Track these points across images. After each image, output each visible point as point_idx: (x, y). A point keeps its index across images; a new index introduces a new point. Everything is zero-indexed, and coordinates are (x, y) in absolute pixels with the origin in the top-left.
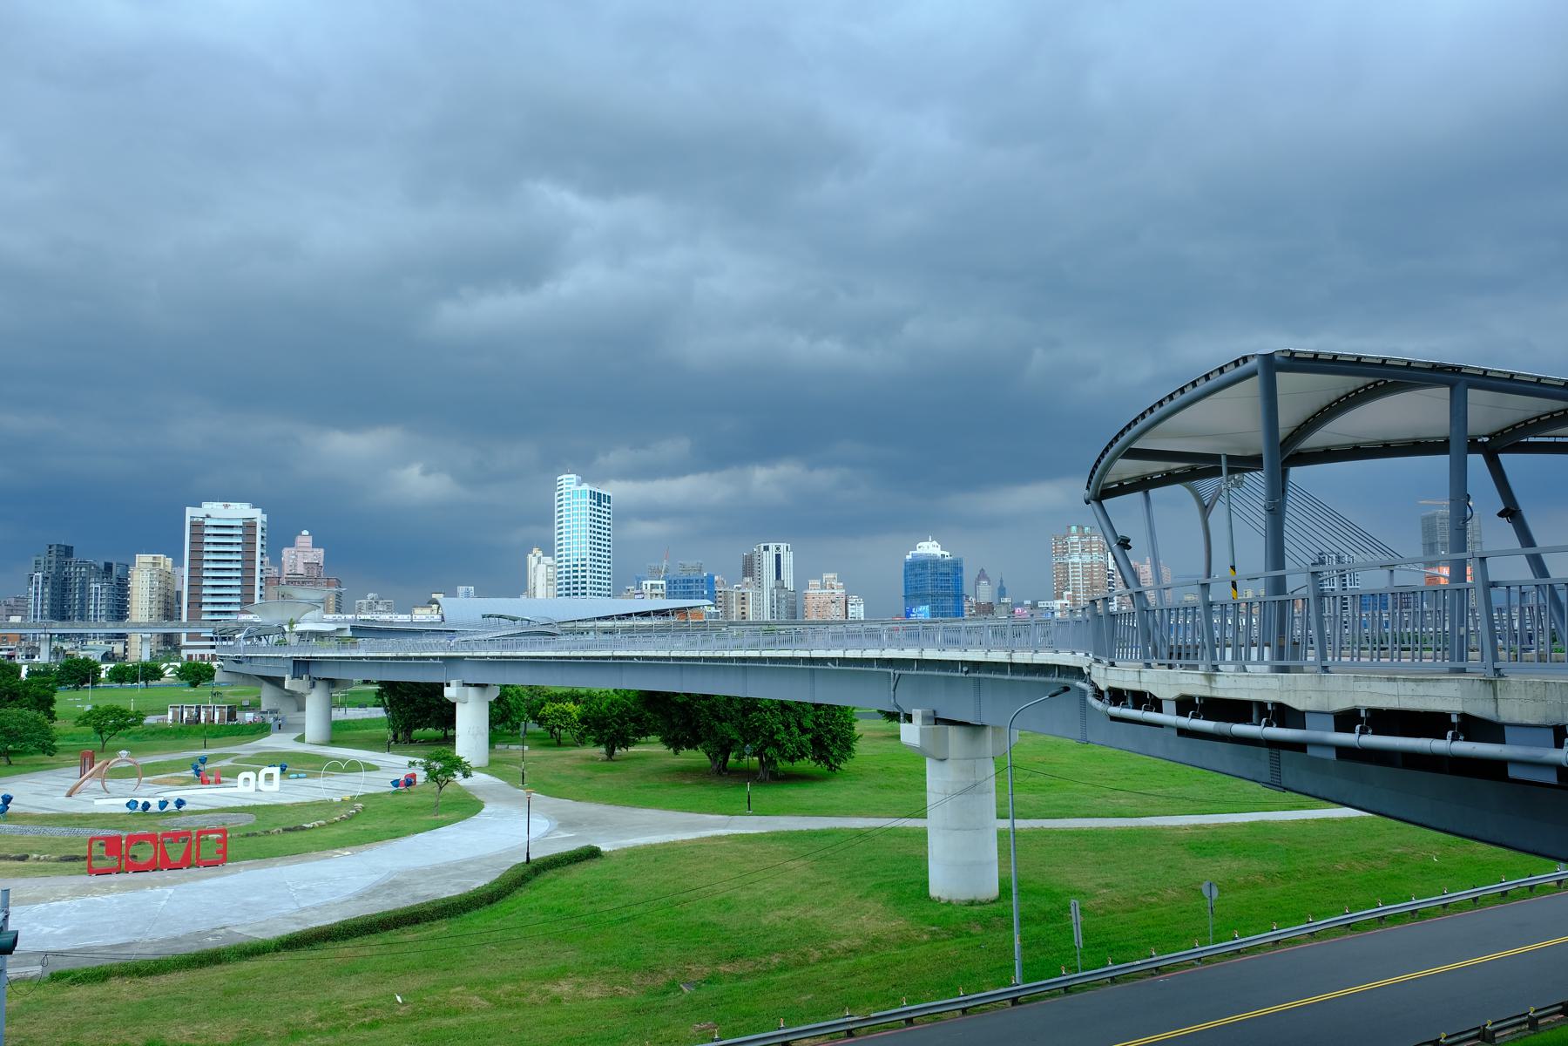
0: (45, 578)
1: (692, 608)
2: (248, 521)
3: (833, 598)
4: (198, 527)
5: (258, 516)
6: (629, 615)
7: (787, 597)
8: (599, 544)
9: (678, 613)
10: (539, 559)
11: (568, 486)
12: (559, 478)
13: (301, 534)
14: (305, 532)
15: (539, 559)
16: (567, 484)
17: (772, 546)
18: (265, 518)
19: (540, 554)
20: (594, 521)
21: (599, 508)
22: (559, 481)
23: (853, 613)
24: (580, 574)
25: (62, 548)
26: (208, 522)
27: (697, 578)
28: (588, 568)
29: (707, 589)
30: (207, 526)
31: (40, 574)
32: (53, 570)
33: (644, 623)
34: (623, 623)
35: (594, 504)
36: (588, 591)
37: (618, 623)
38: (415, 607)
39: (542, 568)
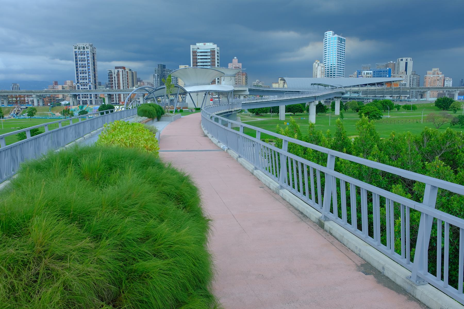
0: (158, 75)
1: (393, 81)
2: (212, 50)
3: (438, 78)
4: (194, 52)
5: (215, 46)
6: (366, 85)
7: (417, 79)
8: (341, 58)
9: (387, 84)
10: (318, 64)
11: (329, 36)
12: (325, 33)
13: (234, 58)
14: (235, 58)
15: (318, 64)
16: (328, 35)
17: (404, 59)
18: (218, 48)
19: (319, 62)
20: (339, 49)
21: (341, 44)
22: (325, 36)
23: (447, 85)
24: (333, 70)
25: (162, 66)
26: (198, 51)
27: (384, 70)
28: (336, 68)
29: (388, 75)
30: (198, 52)
31: (156, 74)
32: (160, 73)
33: (372, 88)
34: (363, 88)
35: (339, 42)
36: (336, 76)
37: (361, 88)
38: (273, 83)
39: (319, 67)
